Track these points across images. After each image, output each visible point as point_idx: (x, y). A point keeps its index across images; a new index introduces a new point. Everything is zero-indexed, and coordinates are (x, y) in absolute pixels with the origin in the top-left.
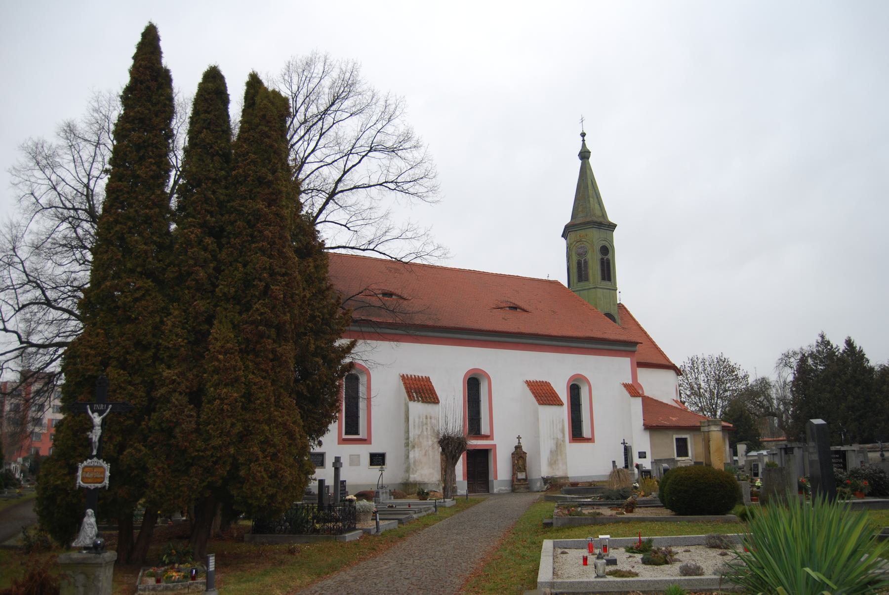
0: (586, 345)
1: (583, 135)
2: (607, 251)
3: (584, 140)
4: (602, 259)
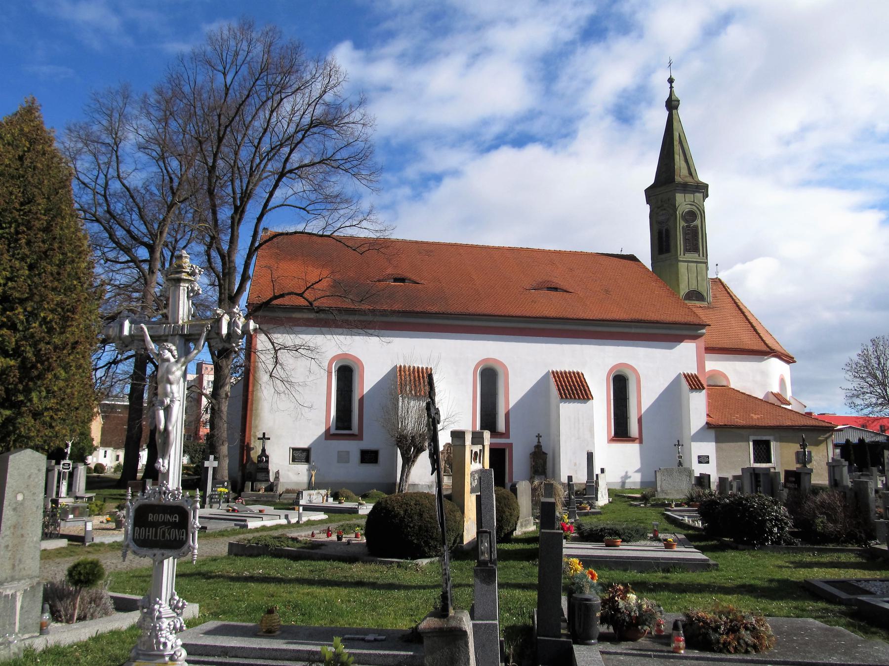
0: (633, 330)
2: (695, 216)
3: (671, 87)
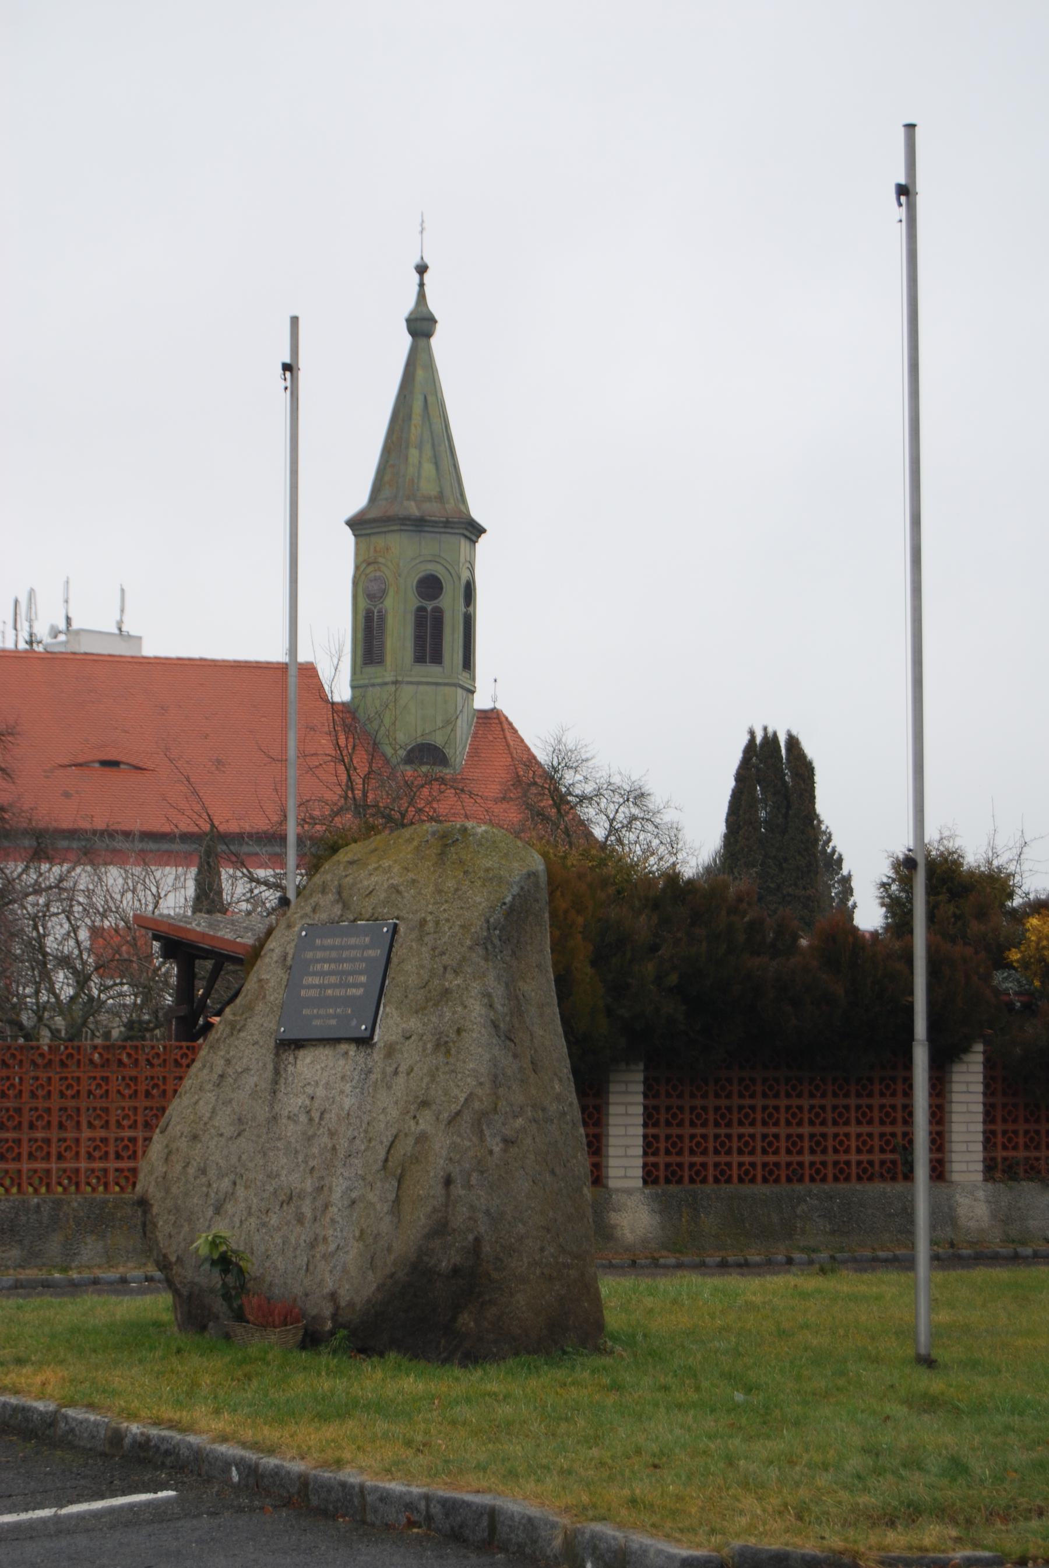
1: (422, 269)
3: (422, 285)
4: (421, 609)
